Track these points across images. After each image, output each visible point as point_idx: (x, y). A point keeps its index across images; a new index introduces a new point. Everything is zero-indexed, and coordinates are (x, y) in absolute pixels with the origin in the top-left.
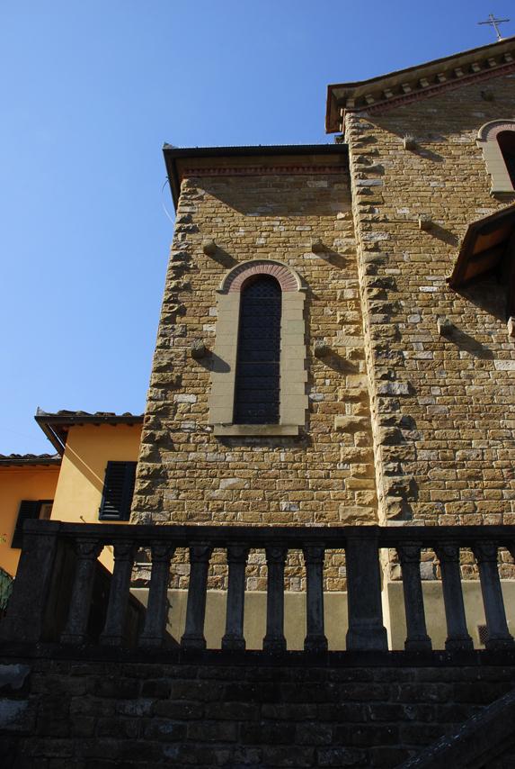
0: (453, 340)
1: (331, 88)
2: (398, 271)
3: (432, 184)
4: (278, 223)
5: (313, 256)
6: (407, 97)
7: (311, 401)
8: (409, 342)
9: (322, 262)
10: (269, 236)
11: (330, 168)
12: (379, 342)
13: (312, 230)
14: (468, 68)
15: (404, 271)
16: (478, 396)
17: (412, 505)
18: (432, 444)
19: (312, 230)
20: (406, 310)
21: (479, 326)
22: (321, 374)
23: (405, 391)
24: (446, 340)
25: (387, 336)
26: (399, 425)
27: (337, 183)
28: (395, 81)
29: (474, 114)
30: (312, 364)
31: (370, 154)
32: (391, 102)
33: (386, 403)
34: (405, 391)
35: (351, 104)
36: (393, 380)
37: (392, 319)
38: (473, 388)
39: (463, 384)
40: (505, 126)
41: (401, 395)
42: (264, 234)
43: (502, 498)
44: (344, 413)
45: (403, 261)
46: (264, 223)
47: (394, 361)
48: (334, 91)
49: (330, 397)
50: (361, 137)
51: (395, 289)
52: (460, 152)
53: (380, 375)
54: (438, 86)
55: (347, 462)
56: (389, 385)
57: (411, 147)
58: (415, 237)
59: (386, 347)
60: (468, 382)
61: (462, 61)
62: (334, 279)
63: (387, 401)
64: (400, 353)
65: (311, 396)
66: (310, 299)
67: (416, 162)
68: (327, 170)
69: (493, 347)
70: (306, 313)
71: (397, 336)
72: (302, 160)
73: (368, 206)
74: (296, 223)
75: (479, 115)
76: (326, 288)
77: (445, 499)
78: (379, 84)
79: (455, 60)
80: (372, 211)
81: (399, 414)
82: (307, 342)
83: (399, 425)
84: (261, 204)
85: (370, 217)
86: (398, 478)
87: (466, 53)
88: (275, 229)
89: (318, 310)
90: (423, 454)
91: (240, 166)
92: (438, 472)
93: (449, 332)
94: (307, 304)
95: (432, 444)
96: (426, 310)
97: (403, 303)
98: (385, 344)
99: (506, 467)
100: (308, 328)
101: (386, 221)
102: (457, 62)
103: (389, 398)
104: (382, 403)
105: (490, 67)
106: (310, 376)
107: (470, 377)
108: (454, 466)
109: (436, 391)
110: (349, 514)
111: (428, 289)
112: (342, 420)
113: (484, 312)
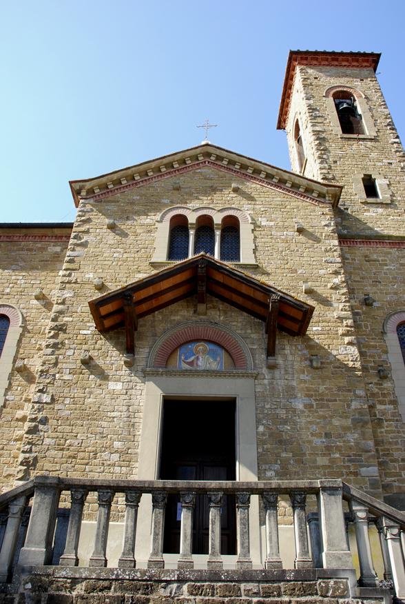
0: (88, 368)
2: (71, 319)
3: (115, 255)
4: (21, 277)
5: (35, 302)
6: (123, 187)
7: (6, 400)
8: (62, 368)
9: (40, 306)
10: (13, 287)
12: (44, 368)
13: (40, 283)
14: (170, 165)
15: (75, 319)
16: (91, 406)
17: (32, 472)
18: (54, 435)
19: (40, 283)
20: (67, 346)
21: (108, 358)
22: (17, 383)
23: (49, 400)
24: (84, 368)
25: (49, 364)
26: (39, 422)
28: (115, 177)
29: (163, 201)
30: (13, 376)
31: (83, 232)
32: (111, 191)
33: (36, 407)
34: (49, 400)
35: (84, 193)
36: (44, 393)
37: (57, 352)
38: (90, 400)
39: (85, 398)
40: (174, 211)
41: (46, 403)
42: (11, 285)
43: (84, 471)
44: (23, 409)
45: (77, 312)
46: (13, 277)
47: (48, 381)
49: (17, 398)
50: (83, 218)
51: (65, 331)
52: (142, 231)
53: (37, 390)
54: (146, 178)
55: (16, 440)
56: (40, 396)
57: (112, 227)
58: (90, 295)
59: (47, 371)
60: (88, 396)
61: (165, 161)
62: (43, 319)
63: (36, 406)
64: (54, 375)
65: (7, 397)
66: (25, 329)
67: (111, 238)
69: (111, 373)
70: (20, 341)
71: (56, 364)
72: (49, 232)
73: (68, 272)
74: (32, 278)
75: (166, 201)
76: (36, 325)
77: (51, 469)
78: (104, 180)
79: (161, 160)
80: (70, 275)
81: (40, 416)
82: (14, 361)
83: (39, 422)
84: (16, 263)
85: (67, 279)
86: (27, 455)
87: (169, 156)
88: (19, 282)
89: (28, 340)
90: (47, 441)
91: (10, 235)
92: (53, 453)
93: (87, 363)
94: (22, 335)
95: (54, 435)
96: (79, 346)
97: (66, 341)
98: (47, 369)
99: (93, 452)
100: (17, 352)
101: (76, 282)
102: (162, 162)
103: (38, 405)
104: (33, 407)
105: (186, 164)
106: (10, 384)
107: (91, 393)
108: (62, 449)
109: (67, 401)
110: (8, 473)
111: (85, 332)
112: (20, 414)
113: (114, 349)
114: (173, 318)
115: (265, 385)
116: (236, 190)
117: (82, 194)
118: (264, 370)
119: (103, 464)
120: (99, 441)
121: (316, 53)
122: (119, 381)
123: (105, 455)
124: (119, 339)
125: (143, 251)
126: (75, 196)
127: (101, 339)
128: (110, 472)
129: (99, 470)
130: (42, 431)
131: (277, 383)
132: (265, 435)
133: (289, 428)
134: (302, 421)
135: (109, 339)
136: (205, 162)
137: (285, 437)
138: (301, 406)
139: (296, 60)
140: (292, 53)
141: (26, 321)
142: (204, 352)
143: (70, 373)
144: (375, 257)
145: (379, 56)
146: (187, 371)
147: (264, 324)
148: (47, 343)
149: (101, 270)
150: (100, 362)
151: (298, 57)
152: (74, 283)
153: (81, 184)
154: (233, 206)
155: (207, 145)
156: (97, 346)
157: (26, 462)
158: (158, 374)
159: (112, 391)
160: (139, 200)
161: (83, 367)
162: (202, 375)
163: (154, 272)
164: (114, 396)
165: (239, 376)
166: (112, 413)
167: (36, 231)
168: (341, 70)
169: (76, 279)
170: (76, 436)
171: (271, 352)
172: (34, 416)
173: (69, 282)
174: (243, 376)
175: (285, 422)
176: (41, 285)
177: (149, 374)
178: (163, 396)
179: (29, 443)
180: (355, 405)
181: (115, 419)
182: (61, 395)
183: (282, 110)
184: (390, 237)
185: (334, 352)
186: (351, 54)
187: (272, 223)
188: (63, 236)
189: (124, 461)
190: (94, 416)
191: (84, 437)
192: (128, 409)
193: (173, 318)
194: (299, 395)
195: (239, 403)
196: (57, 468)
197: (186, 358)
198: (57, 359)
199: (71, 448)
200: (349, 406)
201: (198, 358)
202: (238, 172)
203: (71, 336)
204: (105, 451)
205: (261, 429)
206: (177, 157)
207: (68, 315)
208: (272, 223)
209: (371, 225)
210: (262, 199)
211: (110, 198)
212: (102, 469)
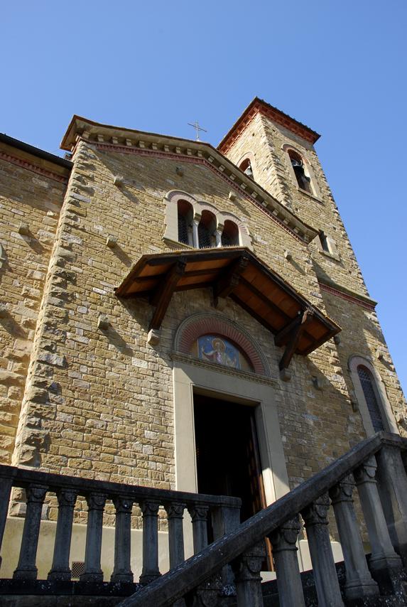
0: (107, 334)
1: (75, 117)
2: (81, 271)
3: (125, 216)
5: (18, 236)
8: (73, 327)
9: (24, 243)
11: (54, 174)
12: (50, 319)
13: (24, 216)
16: (114, 381)
17: (43, 455)
18: (70, 409)
19: (24, 216)
20: (78, 301)
23: (60, 363)
25: (58, 317)
27: (55, 188)
28: (123, 134)
31: (88, 177)
33: (43, 368)
34: (60, 363)
38: (112, 374)
39: (105, 369)
43: (113, 462)
47: (58, 338)
48: (78, 121)
50: (85, 162)
51: (74, 283)
52: (151, 202)
53: (43, 346)
57: (119, 185)
59: (55, 325)
61: (171, 142)
62: (29, 259)
63: (44, 367)
64: (64, 333)
68: (51, 176)
71: (66, 320)
72: (36, 160)
76: (21, 264)
78: (111, 131)
79: (167, 139)
81: (51, 380)
83: (48, 389)
86: (36, 431)
87: (175, 139)
90: (61, 416)
92: (69, 432)
93: (105, 327)
95: (70, 409)
96: (93, 306)
98: (55, 322)
99: (121, 439)
103: (46, 366)
104: (39, 368)
105: (197, 156)
107: (112, 365)
108: (83, 431)
111: (99, 291)
113: (134, 320)
114: (192, 304)
115: (281, 395)
116: (233, 199)
117: (84, 135)
118: (279, 381)
119: (135, 456)
120: (127, 427)
121: (275, 110)
122: (143, 358)
123: (136, 445)
124: (138, 310)
125: (154, 223)
126: (72, 131)
127: (118, 304)
128: (144, 468)
129: (130, 463)
130: (53, 401)
131: (290, 397)
132: (288, 446)
133: (306, 442)
134: (315, 437)
135: (128, 307)
136: (202, 160)
137: (304, 451)
138: (311, 423)
139: (257, 108)
140: (257, 100)
141: (6, 255)
142: (222, 348)
143: (84, 335)
144: (334, 302)
145: (319, 136)
146: (203, 361)
147: (273, 336)
148: (53, 290)
149: (111, 227)
150: (119, 330)
151: (259, 105)
152: (81, 229)
153: (87, 124)
154: (232, 213)
155: (209, 145)
156: (114, 311)
157: (34, 440)
158: (186, 361)
159: (136, 369)
160: (144, 169)
161: (99, 331)
162: (229, 373)
163: (168, 250)
164: (140, 376)
165: (261, 382)
166: (140, 395)
167: (19, 153)
168: (290, 133)
169: (84, 226)
170: (99, 416)
171: (283, 364)
172: (41, 380)
173: (76, 227)
174: (265, 382)
175: (302, 435)
176: (24, 219)
177: (177, 359)
178: (193, 386)
179: (36, 415)
180: (350, 429)
181: (143, 403)
182: (75, 360)
183: (227, 137)
184: (344, 290)
185: (329, 378)
186: (300, 124)
187: (266, 243)
188: (50, 173)
189: (158, 455)
190: (119, 395)
191: (105, 417)
192: (157, 394)
193: (192, 304)
194: (309, 412)
195: (264, 408)
196: (78, 454)
197: (206, 351)
198: (67, 313)
199: (94, 431)
200: (346, 429)
201: (216, 354)
202: (232, 183)
203: (83, 290)
204: (135, 440)
205: (284, 439)
206: (182, 144)
207: (76, 264)
208: (266, 243)
209: (328, 274)
210: (255, 217)
211: (115, 155)
212: (134, 462)
